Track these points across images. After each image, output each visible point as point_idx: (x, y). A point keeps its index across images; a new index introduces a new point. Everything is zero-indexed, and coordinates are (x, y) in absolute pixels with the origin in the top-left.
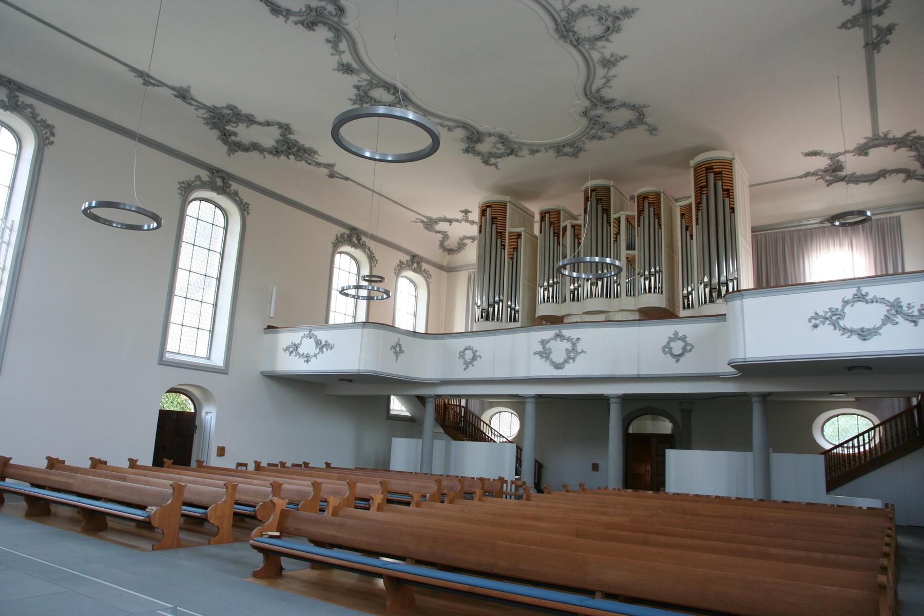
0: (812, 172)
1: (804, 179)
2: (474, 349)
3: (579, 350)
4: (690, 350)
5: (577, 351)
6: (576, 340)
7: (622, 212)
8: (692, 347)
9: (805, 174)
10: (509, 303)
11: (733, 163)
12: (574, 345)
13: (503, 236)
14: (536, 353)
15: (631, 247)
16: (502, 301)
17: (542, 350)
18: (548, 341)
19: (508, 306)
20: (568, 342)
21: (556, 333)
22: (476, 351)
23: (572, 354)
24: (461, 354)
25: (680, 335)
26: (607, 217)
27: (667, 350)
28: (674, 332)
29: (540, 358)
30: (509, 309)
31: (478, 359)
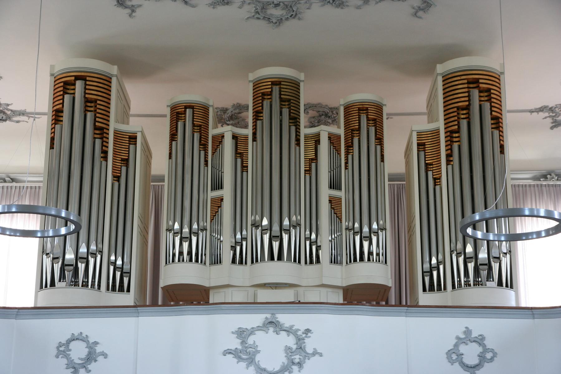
0: (550, 106)
1: (535, 114)
2: (91, 340)
3: (309, 350)
4: (492, 359)
5: (305, 352)
6: (303, 333)
7: (323, 127)
8: (495, 355)
9: (540, 108)
10: (113, 258)
11: (501, 78)
12: (300, 341)
13: (105, 135)
14: (227, 352)
15: (334, 185)
16: (101, 252)
17: (240, 347)
18: (252, 332)
19: (109, 263)
20: (288, 336)
21: (266, 318)
22: (96, 343)
23: (297, 357)
24: (62, 349)
25: (475, 334)
26: (296, 132)
27: (454, 357)
28: (465, 329)
29: (236, 360)
30: (112, 268)
31: (100, 358)
